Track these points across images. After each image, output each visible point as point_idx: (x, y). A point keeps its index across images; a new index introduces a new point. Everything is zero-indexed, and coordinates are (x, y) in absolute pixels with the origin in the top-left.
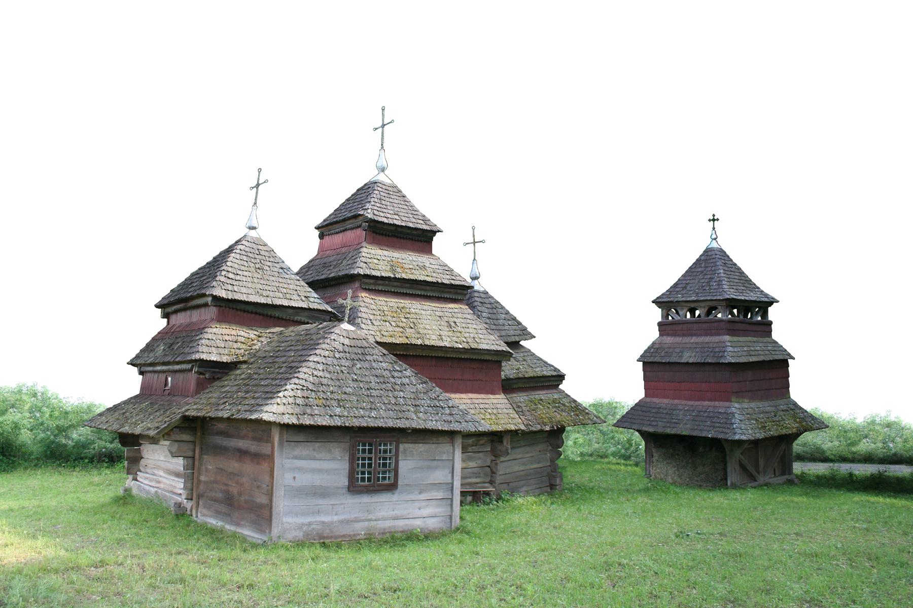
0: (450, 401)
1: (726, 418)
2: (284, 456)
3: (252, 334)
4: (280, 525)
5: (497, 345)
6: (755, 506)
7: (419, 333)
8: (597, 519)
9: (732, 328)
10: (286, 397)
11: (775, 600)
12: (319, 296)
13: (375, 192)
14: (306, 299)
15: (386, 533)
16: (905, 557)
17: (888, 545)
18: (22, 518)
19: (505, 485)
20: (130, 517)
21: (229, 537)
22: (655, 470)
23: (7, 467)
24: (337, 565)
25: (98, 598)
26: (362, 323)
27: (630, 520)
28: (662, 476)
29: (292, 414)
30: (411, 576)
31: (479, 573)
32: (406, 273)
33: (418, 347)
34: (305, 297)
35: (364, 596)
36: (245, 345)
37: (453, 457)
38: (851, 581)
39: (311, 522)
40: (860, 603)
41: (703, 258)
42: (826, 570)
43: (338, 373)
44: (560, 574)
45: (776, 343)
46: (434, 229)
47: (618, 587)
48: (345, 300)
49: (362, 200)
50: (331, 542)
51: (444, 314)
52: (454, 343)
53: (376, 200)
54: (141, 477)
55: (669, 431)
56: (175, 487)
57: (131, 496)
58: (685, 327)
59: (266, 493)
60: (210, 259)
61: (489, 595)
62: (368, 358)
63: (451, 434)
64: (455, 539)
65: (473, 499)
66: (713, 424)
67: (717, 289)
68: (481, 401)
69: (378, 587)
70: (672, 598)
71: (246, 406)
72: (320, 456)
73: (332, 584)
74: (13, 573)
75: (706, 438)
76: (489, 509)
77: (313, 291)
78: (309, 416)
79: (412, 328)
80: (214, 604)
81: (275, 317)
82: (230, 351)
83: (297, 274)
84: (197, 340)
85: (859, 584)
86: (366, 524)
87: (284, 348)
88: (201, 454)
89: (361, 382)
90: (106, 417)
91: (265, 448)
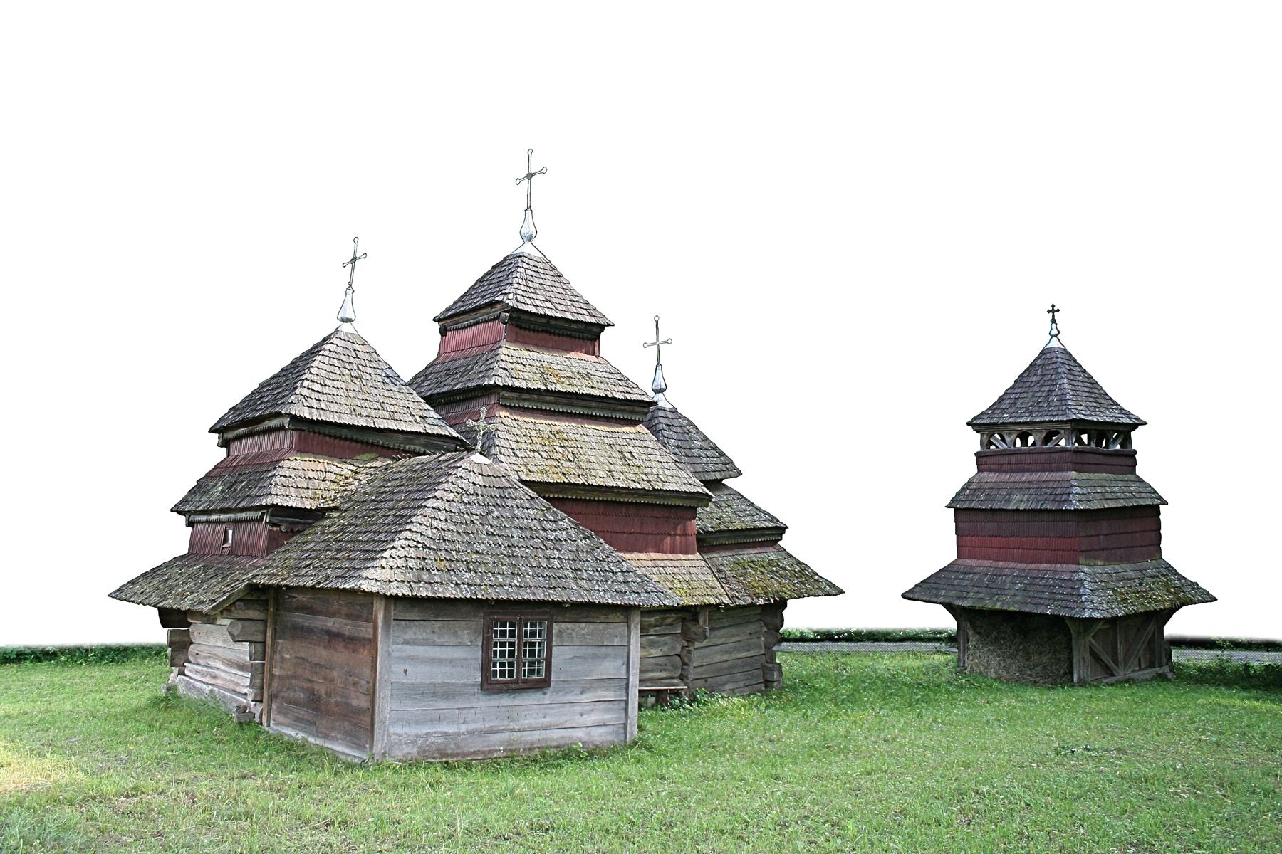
0: (624, 563)
1: (1071, 588)
2: (391, 641)
3: (346, 469)
4: (385, 737)
5: (690, 484)
6: (1167, 711)
7: (580, 468)
8: (945, 728)
9: (1079, 460)
10: (394, 558)
11: (1089, 842)
12: (440, 415)
13: (519, 269)
14: (422, 420)
15: (535, 748)
16: (1270, 783)
17: (1246, 766)
18: (24, 727)
19: (702, 682)
20: (175, 726)
21: (314, 754)
22: (972, 660)
23: (117, 656)
24: (465, 793)
25: (130, 841)
26: (501, 453)
27: (991, 730)
28: (982, 668)
29: (403, 581)
30: (570, 808)
31: (779, 805)
32: (563, 383)
33: (578, 487)
34: (420, 417)
35: (504, 837)
36: (336, 484)
37: (629, 642)
38: (1194, 816)
39: (429, 733)
40: (1207, 846)
41: (1038, 362)
42: (1160, 801)
43: (466, 524)
44: (893, 806)
45: (1141, 481)
46: (602, 322)
47: (974, 825)
48: (476, 421)
49: (501, 281)
50: (456, 761)
51: (616, 441)
52: (630, 482)
53: (520, 281)
54: (190, 671)
55: (989, 605)
56: (238, 684)
57: (175, 696)
58: (1013, 459)
59: (365, 693)
60: (286, 362)
61: (794, 836)
62: (509, 502)
63: (627, 609)
64: (632, 757)
65: (657, 701)
66: (1053, 596)
67: (1059, 406)
68: (668, 563)
69: (524, 824)
70: (1050, 839)
71: (337, 570)
72: (442, 640)
73: (458, 821)
74: (10, 804)
75: (1044, 615)
76: (679, 715)
77: (431, 409)
78: (427, 585)
79: (571, 461)
80: (293, 849)
81: (378, 446)
82: (316, 494)
83: (409, 384)
84: (269, 477)
85: (1206, 820)
86: (506, 735)
87: (391, 489)
88: (274, 637)
89: (499, 536)
90: (141, 585)
91: (364, 630)
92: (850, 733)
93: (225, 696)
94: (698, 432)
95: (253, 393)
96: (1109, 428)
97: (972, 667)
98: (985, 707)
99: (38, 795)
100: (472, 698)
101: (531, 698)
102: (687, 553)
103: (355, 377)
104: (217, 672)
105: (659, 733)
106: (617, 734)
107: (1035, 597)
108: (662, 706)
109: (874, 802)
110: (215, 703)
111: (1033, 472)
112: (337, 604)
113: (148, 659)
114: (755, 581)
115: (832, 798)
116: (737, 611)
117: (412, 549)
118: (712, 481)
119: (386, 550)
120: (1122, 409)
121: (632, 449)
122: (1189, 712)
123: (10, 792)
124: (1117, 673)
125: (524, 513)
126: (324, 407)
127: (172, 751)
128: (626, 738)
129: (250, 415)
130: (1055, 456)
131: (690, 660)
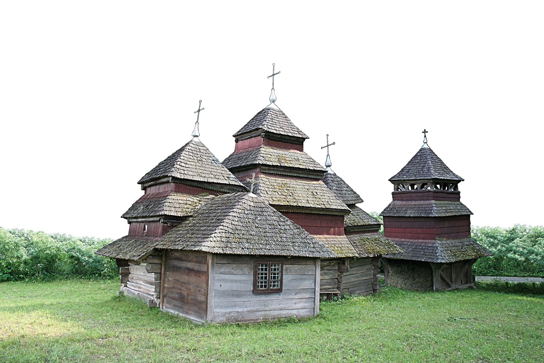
0: (313, 239)
1: (433, 250)
2: (215, 272)
3: (196, 199)
4: (212, 313)
7: (295, 199)
8: (401, 309)
9: (436, 195)
11: (462, 358)
13: (269, 115)
15: (275, 318)
16: (539, 333)
19: (346, 290)
20: (123, 309)
22: (391, 281)
24: (246, 337)
26: (261, 193)
27: (421, 310)
29: (220, 247)
30: (290, 344)
31: (330, 342)
32: (287, 163)
34: (227, 177)
37: (316, 273)
41: (419, 154)
43: (247, 223)
45: (462, 204)
46: (304, 137)
48: (251, 179)
51: (310, 188)
53: (269, 119)
54: (129, 285)
56: (150, 291)
57: (123, 296)
58: (408, 195)
60: (170, 154)
61: (337, 355)
62: (265, 214)
63: (315, 259)
64: (317, 322)
65: (327, 298)
68: (332, 239)
69: (271, 351)
70: (446, 357)
71: (192, 242)
74: (53, 342)
76: (337, 304)
78: (230, 249)
79: (291, 196)
81: (209, 189)
82: (183, 210)
83: (222, 163)
85: (512, 349)
87: (214, 208)
88: (165, 271)
89: (260, 228)
90: (108, 249)
92: (361, 311)
93: (144, 296)
94: (345, 183)
95: (156, 167)
96: (449, 182)
97: (390, 284)
98: (418, 300)
99: (65, 338)
100: (249, 297)
101: (274, 297)
102: (340, 235)
103: (199, 160)
104: (141, 286)
105: (328, 312)
106: (311, 312)
107: (417, 254)
108: (330, 300)
109: (371, 341)
110: (140, 299)
111: (416, 200)
112: (191, 257)
113: (63, 280)
114: (369, 247)
115: (353, 339)
116: (361, 260)
117: (223, 234)
118: (351, 204)
119: (212, 234)
120: (454, 174)
121: (317, 191)
122: (505, 303)
123: (53, 337)
124: (452, 286)
125: (271, 218)
126: (186, 173)
127: (122, 319)
128: (314, 314)
129: (154, 177)
130: (426, 194)
131: (341, 281)
